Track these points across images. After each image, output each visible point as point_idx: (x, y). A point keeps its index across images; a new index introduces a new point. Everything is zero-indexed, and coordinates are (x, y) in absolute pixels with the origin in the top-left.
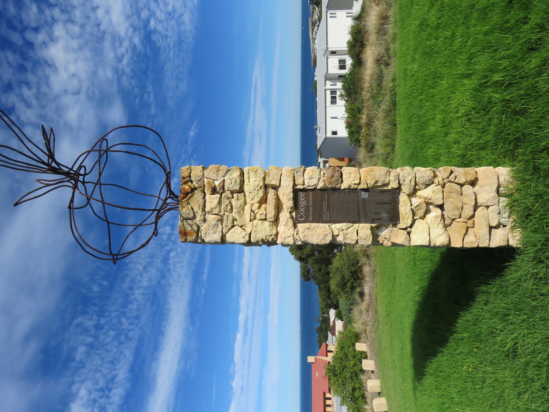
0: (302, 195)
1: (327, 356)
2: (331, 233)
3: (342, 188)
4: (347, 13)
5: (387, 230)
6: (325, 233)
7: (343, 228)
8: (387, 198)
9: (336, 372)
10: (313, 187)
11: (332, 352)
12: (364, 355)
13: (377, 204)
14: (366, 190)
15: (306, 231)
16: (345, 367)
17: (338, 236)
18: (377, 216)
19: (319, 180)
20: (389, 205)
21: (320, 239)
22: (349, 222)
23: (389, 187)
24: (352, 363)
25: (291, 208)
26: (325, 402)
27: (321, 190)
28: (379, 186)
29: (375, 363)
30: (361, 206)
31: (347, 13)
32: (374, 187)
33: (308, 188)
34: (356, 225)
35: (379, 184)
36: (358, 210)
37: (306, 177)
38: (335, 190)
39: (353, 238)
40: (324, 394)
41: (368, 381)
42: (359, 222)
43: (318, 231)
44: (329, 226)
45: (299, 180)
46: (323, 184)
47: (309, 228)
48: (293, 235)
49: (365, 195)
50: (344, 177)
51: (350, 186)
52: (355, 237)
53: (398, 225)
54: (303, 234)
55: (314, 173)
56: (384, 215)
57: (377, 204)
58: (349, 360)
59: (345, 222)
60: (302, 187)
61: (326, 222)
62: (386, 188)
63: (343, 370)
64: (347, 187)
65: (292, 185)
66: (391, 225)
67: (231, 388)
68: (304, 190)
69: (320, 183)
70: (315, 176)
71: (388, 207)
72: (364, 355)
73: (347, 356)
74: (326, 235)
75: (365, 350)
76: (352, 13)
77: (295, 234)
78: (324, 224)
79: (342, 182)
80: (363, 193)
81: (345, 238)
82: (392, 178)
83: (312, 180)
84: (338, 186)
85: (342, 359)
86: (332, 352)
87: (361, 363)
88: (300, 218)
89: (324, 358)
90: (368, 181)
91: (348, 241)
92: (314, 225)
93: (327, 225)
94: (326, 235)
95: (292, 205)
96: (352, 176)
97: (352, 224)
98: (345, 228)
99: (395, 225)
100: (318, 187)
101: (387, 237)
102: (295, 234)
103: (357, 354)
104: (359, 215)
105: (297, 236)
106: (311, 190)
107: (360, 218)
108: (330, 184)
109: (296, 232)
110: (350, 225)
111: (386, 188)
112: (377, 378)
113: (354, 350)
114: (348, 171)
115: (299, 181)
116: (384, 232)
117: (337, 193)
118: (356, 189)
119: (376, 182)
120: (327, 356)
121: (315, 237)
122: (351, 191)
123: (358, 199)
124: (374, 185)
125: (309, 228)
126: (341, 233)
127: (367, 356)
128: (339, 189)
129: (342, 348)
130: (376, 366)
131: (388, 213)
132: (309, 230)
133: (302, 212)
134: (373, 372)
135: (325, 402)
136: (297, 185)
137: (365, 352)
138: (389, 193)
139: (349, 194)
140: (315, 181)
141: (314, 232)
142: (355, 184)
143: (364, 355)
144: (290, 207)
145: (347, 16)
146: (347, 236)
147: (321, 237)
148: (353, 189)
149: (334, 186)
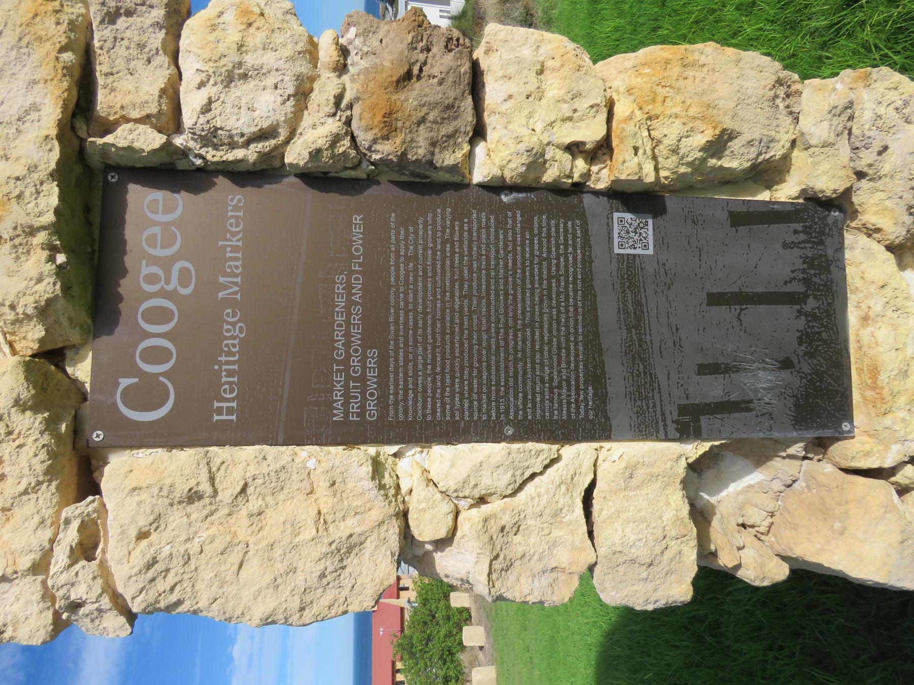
0: (149, 213)
1: (398, 597)
2: (393, 532)
3: (478, 176)
4: (441, 11)
5: (755, 477)
6: (340, 531)
7: (486, 482)
8: (772, 262)
9: (414, 650)
10: (250, 154)
11: (407, 589)
12: (465, 615)
13: (715, 299)
14: (638, 199)
15: (176, 518)
16: (429, 639)
17: (442, 544)
18: (714, 389)
19: (302, 94)
20: (786, 312)
21: (299, 580)
22: (527, 431)
23: (786, 192)
24: (443, 632)
25: (44, 311)
26: (394, 676)
27: (319, 177)
28: (729, 180)
29: (487, 632)
30: (608, 310)
31: (441, 11)
32: (702, 180)
33: (213, 156)
34: (577, 455)
35: (735, 160)
36: (593, 343)
37: (189, 65)
38: (423, 182)
39: (563, 557)
40: (393, 663)
41: (474, 671)
42: (598, 429)
43: (273, 518)
44: (377, 467)
45: (126, 84)
46: (333, 126)
47: (193, 497)
48: (40, 567)
49: (632, 237)
50: (493, 92)
51: (538, 162)
52: (571, 551)
53: (836, 449)
54: (141, 553)
55: (256, 38)
56: (762, 381)
57: (715, 299)
58: (437, 624)
59: (495, 436)
60: (148, 140)
61: (349, 435)
62: (764, 196)
63: (427, 644)
64: (513, 169)
65: (51, 113)
66: (797, 449)
67: (231, 659)
68: (170, 171)
69: (307, 119)
70: (269, 59)
71: (784, 321)
72: (465, 615)
73: (434, 617)
74: (350, 547)
75: (467, 605)
76: (449, 12)
77: (61, 557)
78: (336, 451)
79: (479, 133)
80: (623, 218)
81: (499, 564)
82: (815, 124)
83: (240, 90)
84: (449, 158)
85: (425, 623)
86: (407, 589)
87: (461, 630)
88: (135, 399)
89: (393, 601)
90: (670, 131)
91: (522, 587)
92: (242, 460)
93: (354, 461)
94: (350, 547)
95: (48, 288)
96: (554, 87)
97: (547, 449)
98: (502, 481)
99: (820, 446)
100: (296, 154)
101: (755, 516)
102: (61, 557)
103: (453, 615)
104: (597, 378)
105: (85, 569)
106: (242, 175)
107: (602, 398)
108: (388, 129)
109: (71, 536)
110: (535, 451)
111: (764, 196)
112: (492, 662)
113: (448, 607)
114: (526, 53)
115: (128, 89)
116: (734, 488)
117: (440, 212)
118: (579, 188)
119: (717, 146)
120: (398, 597)
121: (252, 569)
122: (543, 198)
123: (588, 261)
124: (697, 166)
125: (193, 497)
126: (471, 518)
127: (470, 617)
128: (455, 183)
129: (425, 602)
130: (487, 637)
131: (786, 364)
132: (196, 510)
133: (156, 355)
134: (481, 648)
135: (394, 676)
136: (108, 128)
137: (467, 610)
138: (784, 231)
139: (527, 224)
140: (261, 104)
141: (241, 524)
142: (574, 149)
143: (465, 617)
144: (28, 304)
145: (441, 17)
146: (519, 544)
147: (309, 565)
148: (556, 189)
149: (420, 152)
